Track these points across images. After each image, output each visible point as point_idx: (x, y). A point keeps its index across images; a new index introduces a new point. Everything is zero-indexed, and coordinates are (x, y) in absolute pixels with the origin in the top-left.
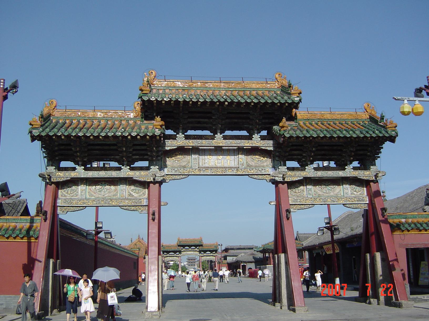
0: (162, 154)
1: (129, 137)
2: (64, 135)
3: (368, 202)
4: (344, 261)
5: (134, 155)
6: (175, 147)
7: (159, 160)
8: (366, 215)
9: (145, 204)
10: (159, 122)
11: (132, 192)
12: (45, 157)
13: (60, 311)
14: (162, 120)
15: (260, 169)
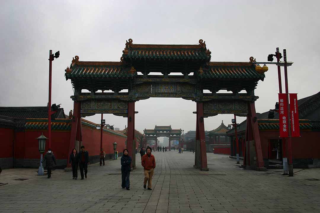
0: (135, 86)
1: (117, 78)
2: (83, 77)
3: (51, 175)
4: (235, 143)
5: (120, 86)
6: (142, 82)
7: (133, 89)
8: (222, 124)
9: (126, 112)
10: (133, 70)
11: (119, 106)
12: (73, 87)
13: (180, 131)
14: (134, 69)
15: (188, 94)
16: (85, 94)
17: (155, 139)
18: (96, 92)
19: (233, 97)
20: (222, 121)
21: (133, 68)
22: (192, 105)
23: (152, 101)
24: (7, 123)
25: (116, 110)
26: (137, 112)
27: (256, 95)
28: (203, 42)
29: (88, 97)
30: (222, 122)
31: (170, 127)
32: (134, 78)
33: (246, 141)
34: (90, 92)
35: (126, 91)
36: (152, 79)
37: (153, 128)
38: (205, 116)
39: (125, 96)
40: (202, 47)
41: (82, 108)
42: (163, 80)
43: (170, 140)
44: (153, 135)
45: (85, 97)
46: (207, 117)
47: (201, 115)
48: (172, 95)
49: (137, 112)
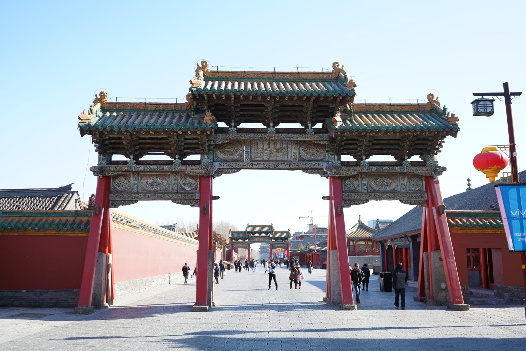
16: (117, 163)
18: (140, 159)
19: (397, 168)
20: (469, 180)
21: (209, 113)
22: (322, 185)
23: (246, 176)
25: (178, 192)
26: (217, 198)
27: (440, 164)
28: (435, 99)
29: (123, 168)
30: (469, 185)
31: (271, 227)
32: (211, 132)
33: (423, 252)
35: (196, 157)
36: (246, 134)
38: (345, 205)
39: (194, 167)
40: (337, 77)
41: (112, 190)
42: (265, 136)
45: (118, 168)
46: (348, 206)
47: (342, 196)
48: (283, 165)
49: (217, 198)
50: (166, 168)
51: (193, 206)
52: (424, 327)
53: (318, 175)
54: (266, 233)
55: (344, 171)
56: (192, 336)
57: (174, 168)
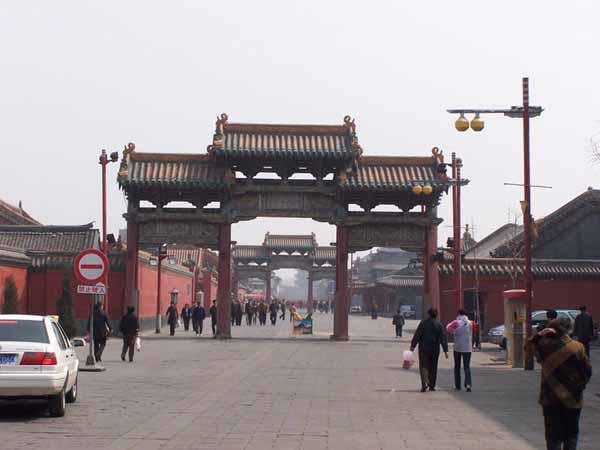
17: (264, 275)
24: (9, 257)
31: (346, 132)
34: (155, 206)
37: (199, 143)
43: (311, 280)
44: (260, 261)
50: (189, 215)
51: (331, 223)
52: (496, 112)
53: (327, 223)
54: (302, 250)
55: (350, 221)
56: (41, 401)
57: (197, 216)
